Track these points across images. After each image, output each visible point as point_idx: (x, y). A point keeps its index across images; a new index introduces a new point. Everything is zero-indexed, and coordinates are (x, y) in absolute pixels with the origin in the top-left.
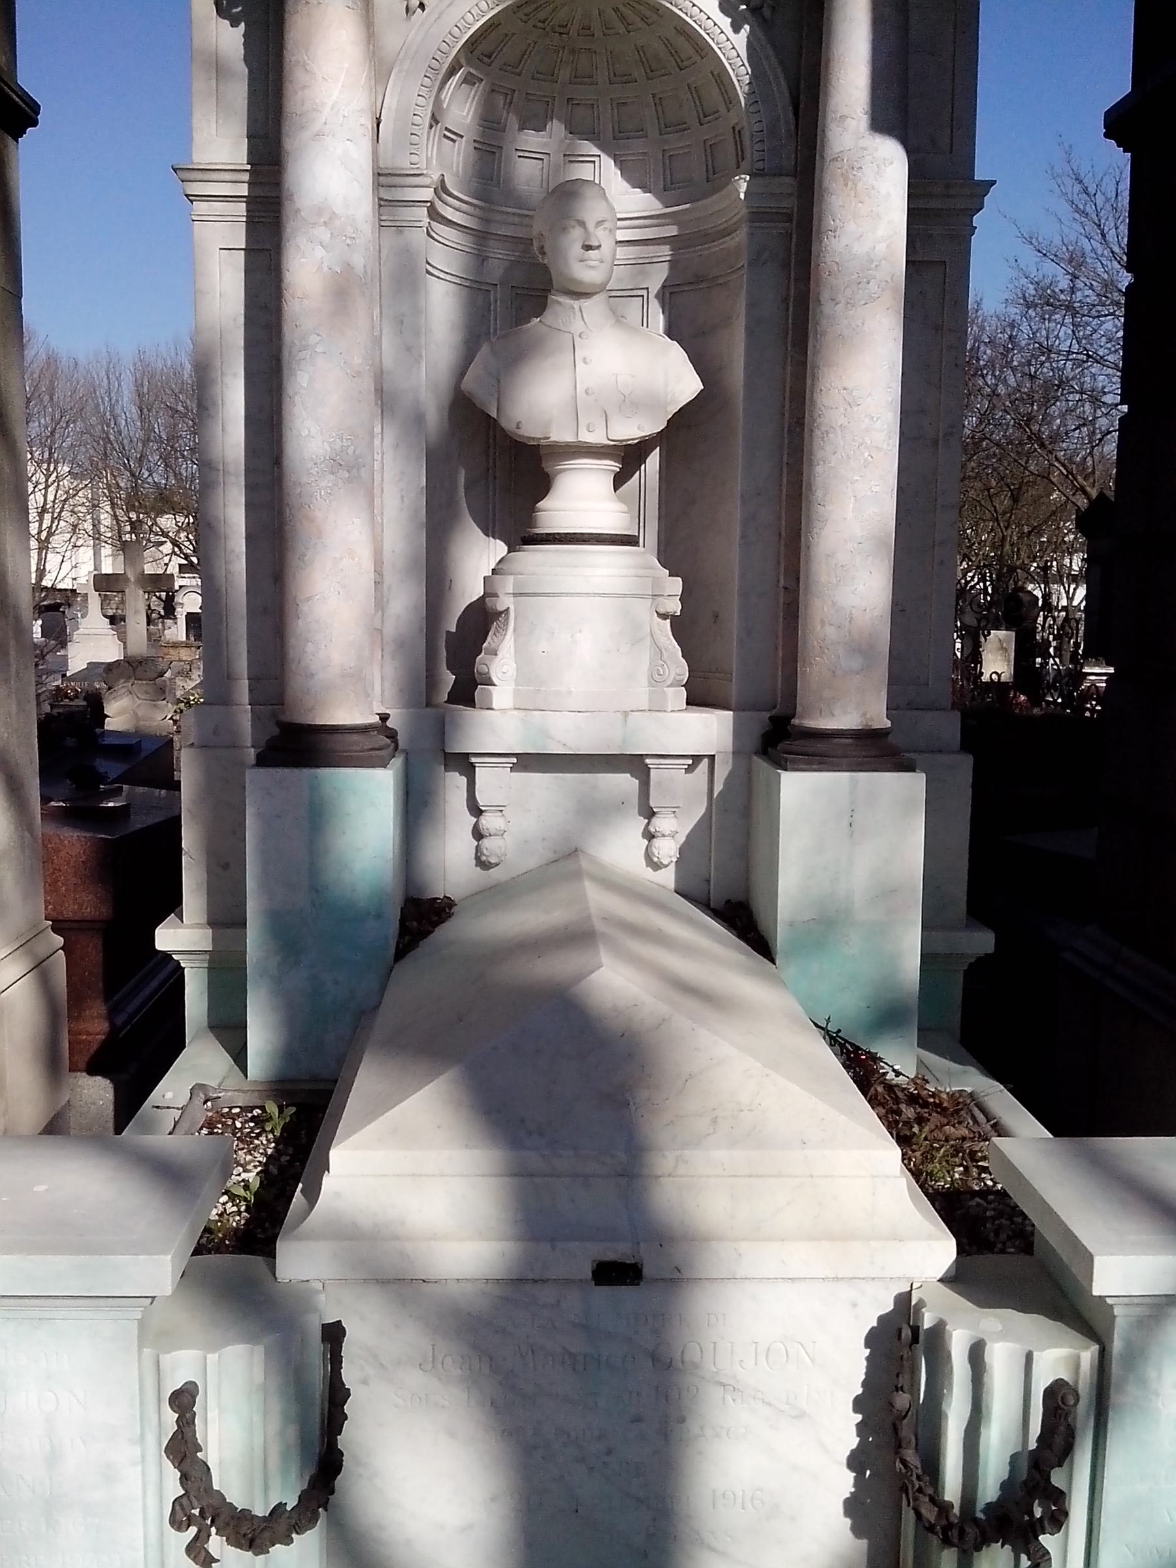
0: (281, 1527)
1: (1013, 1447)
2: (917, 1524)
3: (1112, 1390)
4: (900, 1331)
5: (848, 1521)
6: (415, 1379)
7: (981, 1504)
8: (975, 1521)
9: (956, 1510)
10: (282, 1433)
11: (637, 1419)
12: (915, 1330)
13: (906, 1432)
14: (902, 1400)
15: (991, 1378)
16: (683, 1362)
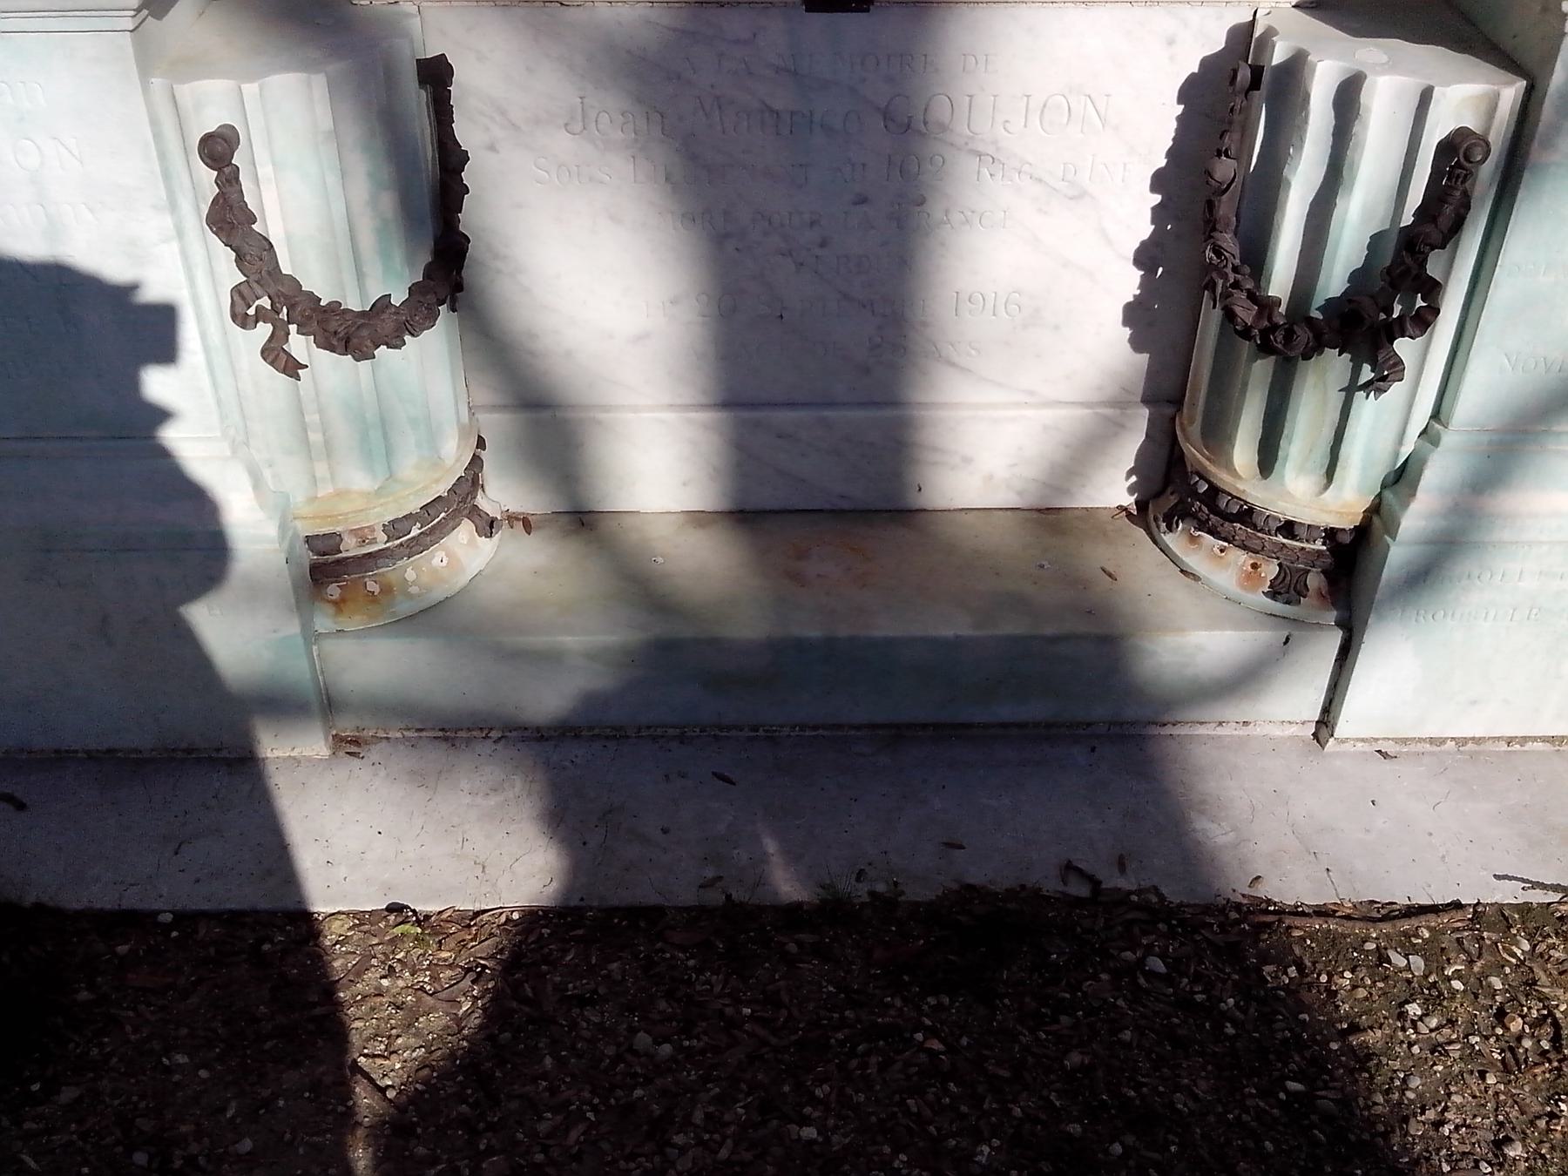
0: (387, 324)
1: (1378, 223)
2: (1222, 326)
3: (1535, 145)
4: (1235, 72)
5: (1127, 331)
6: (562, 144)
7: (1319, 300)
8: (1310, 321)
9: (1282, 309)
10: (373, 202)
11: (862, 200)
12: (1257, 72)
13: (1226, 208)
14: (1224, 169)
15: (1365, 128)
16: (925, 123)
